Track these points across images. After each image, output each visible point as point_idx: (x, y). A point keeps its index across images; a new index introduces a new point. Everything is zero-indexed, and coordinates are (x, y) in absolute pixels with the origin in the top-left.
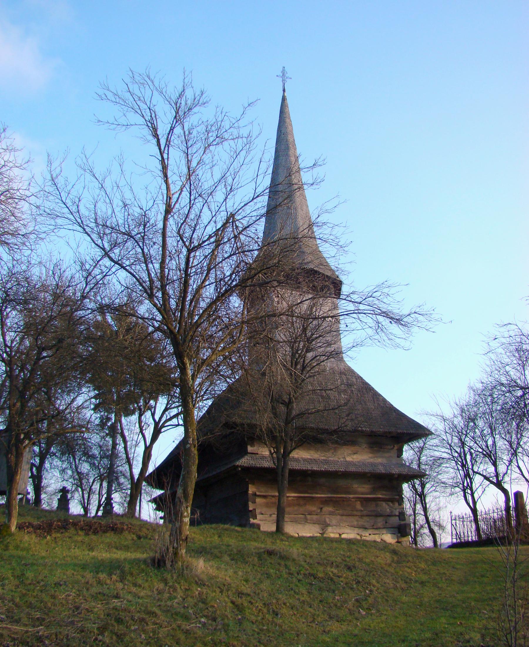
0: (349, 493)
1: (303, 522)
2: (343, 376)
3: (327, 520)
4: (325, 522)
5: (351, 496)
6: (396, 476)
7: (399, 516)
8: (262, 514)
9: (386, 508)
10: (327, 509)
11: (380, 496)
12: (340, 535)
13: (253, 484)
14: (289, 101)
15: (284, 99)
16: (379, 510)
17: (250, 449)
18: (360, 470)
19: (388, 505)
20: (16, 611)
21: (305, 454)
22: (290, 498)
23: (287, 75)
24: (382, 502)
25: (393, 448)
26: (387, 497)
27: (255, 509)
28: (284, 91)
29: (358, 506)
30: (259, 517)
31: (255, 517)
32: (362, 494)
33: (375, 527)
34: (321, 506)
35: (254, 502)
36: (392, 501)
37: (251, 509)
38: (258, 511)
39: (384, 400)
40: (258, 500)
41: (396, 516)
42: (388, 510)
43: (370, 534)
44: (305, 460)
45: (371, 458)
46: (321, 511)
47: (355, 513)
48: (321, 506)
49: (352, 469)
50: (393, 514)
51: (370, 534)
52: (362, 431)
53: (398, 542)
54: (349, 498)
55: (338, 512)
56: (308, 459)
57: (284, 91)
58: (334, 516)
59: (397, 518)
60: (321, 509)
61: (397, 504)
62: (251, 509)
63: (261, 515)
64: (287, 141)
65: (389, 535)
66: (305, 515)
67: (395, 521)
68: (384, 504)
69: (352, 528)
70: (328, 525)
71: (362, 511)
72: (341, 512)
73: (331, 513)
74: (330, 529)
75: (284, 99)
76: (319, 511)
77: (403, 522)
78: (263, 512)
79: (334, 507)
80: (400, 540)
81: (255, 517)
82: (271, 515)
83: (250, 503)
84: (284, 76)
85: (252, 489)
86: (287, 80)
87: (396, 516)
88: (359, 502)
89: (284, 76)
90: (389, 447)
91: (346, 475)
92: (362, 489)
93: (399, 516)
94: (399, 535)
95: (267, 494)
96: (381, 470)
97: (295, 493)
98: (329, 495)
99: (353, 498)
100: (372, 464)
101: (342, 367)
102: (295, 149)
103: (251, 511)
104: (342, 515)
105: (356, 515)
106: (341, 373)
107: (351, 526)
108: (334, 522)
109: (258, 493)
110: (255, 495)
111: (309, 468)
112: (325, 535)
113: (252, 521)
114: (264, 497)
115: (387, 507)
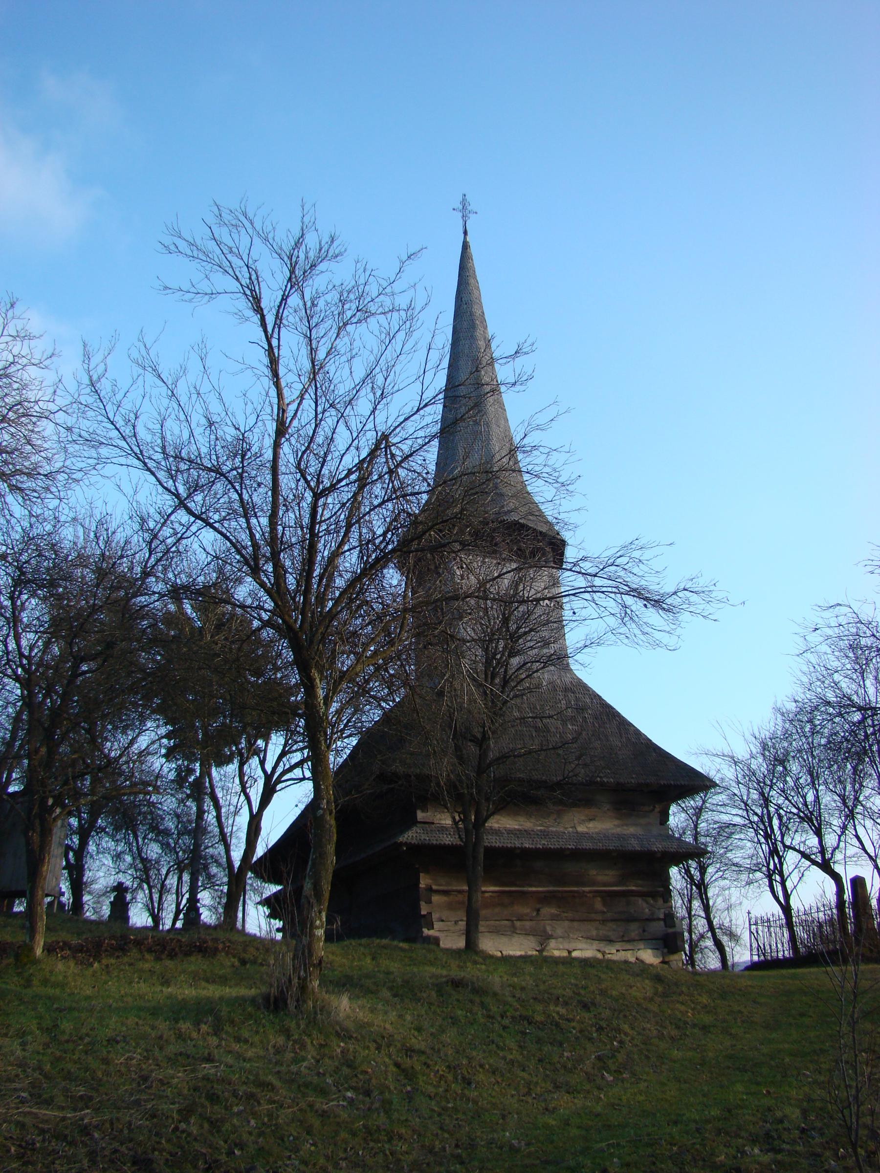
0: (584, 885)
1: (509, 933)
2: (570, 694)
3: (548, 928)
4: (545, 931)
5: (587, 889)
6: (659, 855)
7: (664, 920)
8: (443, 921)
9: (643, 906)
10: (548, 910)
11: (634, 888)
12: (570, 952)
13: (427, 871)
14: (474, 250)
15: (465, 246)
16: (632, 911)
17: (420, 815)
18: (600, 846)
19: (647, 903)
20: (45, 1085)
21: (511, 822)
22: (487, 895)
23: (469, 208)
24: (636, 898)
25: (653, 810)
26: (645, 889)
27: (431, 913)
28: (465, 233)
29: (598, 905)
30: (437, 925)
31: (431, 927)
32: (605, 886)
33: (626, 939)
34: (538, 906)
35: (429, 902)
36: (653, 895)
37: (423, 912)
38: (435, 916)
39: (638, 733)
40: (435, 898)
41: (659, 919)
42: (647, 910)
43: (618, 951)
44: (510, 832)
45: (618, 826)
46: (538, 914)
47: (593, 916)
48: (538, 906)
49: (587, 845)
50: (655, 917)
51: (618, 951)
52: (602, 784)
53: (663, 962)
54: (584, 892)
55: (566, 914)
56: (515, 830)
57: (465, 233)
58: (559, 922)
59: (662, 923)
60: (538, 910)
61: (660, 901)
62: (423, 912)
63: (441, 923)
64: (472, 314)
65: (649, 951)
66: (512, 921)
67: (658, 927)
68: (640, 901)
69: (589, 941)
70: (550, 937)
71: (604, 912)
72: (570, 915)
73: (554, 918)
74: (552, 943)
75: (465, 246)
76: (535, 914)
77: (671, 930)
78: (444, 918)
79: (559, 907)
80: (667, 960)
81: (431, 927)
82: (456, 922)
83: (423, 904)
84: (464, 209)
85: (424, 881)
86: (470, 215)
87: (659, 919)
88: (599, 899)
89: (464, 209)
90: (647, 808)
91: (579, 855)
92: (605, 877)
93: (664, 920)
94: (666, 950)
95: (450, 888)
96: (635, 845)
97: (496, 885)
98: (551, 889)
99: (590, 892)
100: (620, 837)
101: (567, 679)
102: (486, 327)
103: (424, 916)
104: (572, 920)
105: (596, 920)
106: (566, 690)
107: (588, 938)
108: (559, 932)
109: (434, 887)
110: (430, 889)
111: (518, 845)
112: (545, 954)
113: (426, 932)
114: (445, 893)
115: (645, 905)
